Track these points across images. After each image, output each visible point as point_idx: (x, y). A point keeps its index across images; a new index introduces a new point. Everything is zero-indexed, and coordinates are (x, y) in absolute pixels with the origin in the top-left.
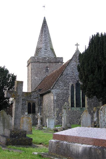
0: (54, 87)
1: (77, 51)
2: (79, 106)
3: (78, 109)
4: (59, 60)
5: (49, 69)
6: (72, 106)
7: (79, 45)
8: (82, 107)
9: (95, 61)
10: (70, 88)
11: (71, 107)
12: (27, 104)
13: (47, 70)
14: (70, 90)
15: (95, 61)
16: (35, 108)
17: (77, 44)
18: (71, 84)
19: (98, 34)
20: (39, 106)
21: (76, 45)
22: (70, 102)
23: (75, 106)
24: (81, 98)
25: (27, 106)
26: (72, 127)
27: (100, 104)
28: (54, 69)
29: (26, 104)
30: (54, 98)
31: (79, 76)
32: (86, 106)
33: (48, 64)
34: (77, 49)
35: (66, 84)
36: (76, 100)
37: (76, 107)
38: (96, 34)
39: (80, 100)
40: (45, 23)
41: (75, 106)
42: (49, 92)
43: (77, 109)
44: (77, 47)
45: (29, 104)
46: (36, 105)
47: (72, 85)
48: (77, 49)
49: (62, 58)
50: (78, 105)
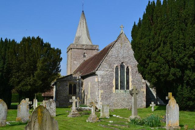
0: (99, 69)
2: (124, 89)
3: (122, 91)
5: (86, 55)
6: (117, 88)
8: (126, 89)
10: (115, 70)
11: (116, 89)
13: (84, 56)
14: (115, 72)
18: (115, 66)
22: (114, 84)
23: (119, 88)
24: (126, 80)
26: (177, 99)
29: (67, 86)
32: (130, 87)
35: (110, 65)
36: (121, 82)
39: (124, 82)
40: (83, 11)
41: (119, 88)
42: (94, 74)
43: (121, 91)
45: (70, 85)
50: (122, 87)
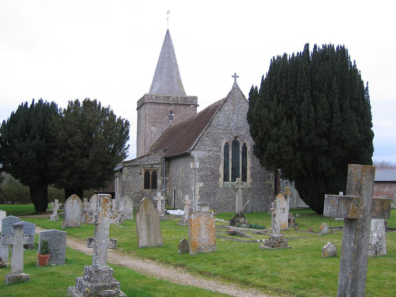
0: (196, 147)
1: (236, 88)
4: (192, 102)
5: (174, 115)
7: (238, 77)
9: (281, 105)
10: (223, 150)
12: (143, 172)
13: (171, 118)
15: (281, 105)
16: (157, 180)
17: (235, 74)
19: (285, 55)
20: (163, 176)
21: (233, 76)
25: (143, 176)
27: (271, 177)
28: (181, 117)
30: (194, 165)
31: (251, 131)
33: (173, 106)
34: (235, 83)
35: (216, 142)
36: (232, 169)
37: (232, 181)
38: (301, 49)
39: (239, 169)
44: (235, 80)
45: (147, 174)
46: (159, 175)
47: (227, 144)
48: (235, 83)
49: (195, 98)
